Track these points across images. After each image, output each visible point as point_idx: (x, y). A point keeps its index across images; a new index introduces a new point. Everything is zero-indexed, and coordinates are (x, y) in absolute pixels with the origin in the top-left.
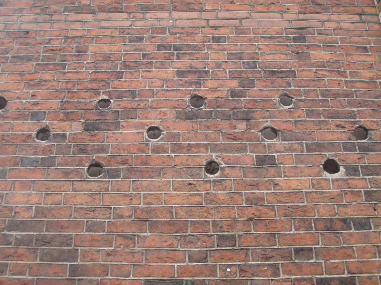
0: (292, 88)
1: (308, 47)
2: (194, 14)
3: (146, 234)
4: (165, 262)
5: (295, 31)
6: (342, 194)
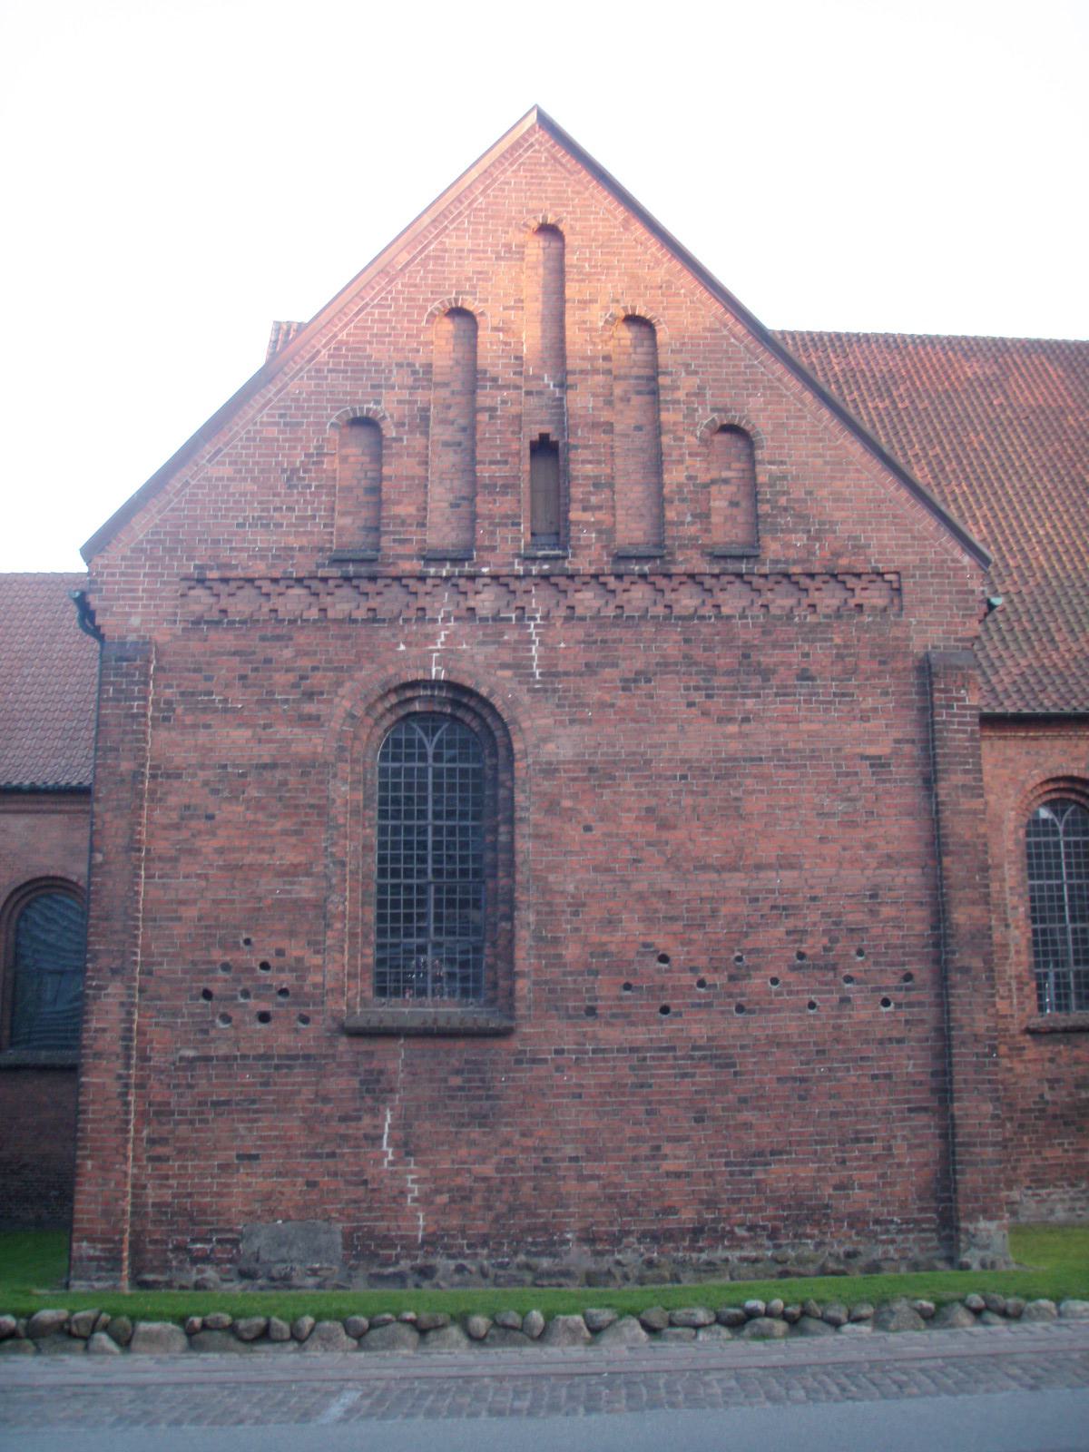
1: (880, 904)
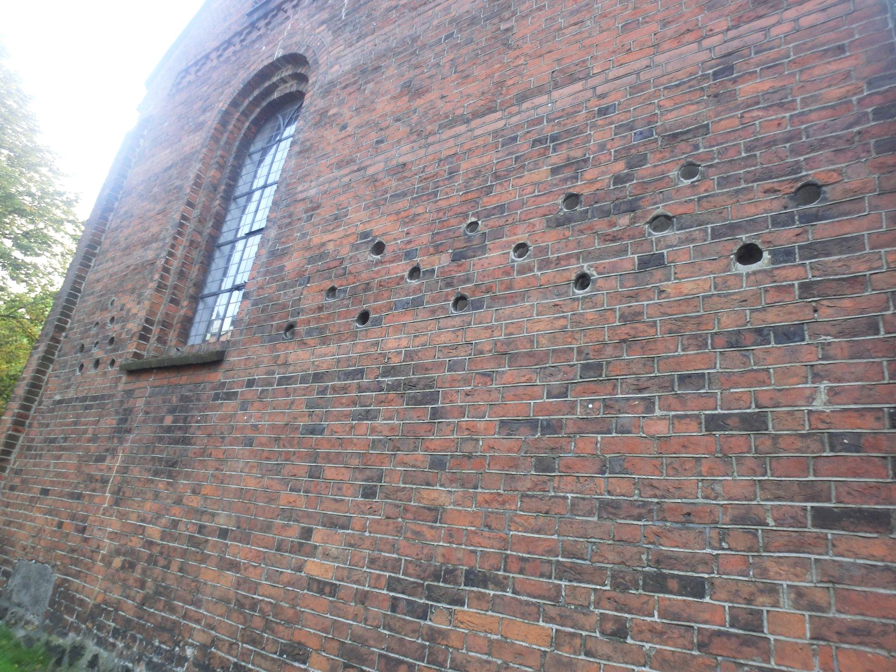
0: (701, 150)
2: (578, 86)
3: (504, 369)
4: (522, 399)
5: (718, 61)
6: (761, 294)
